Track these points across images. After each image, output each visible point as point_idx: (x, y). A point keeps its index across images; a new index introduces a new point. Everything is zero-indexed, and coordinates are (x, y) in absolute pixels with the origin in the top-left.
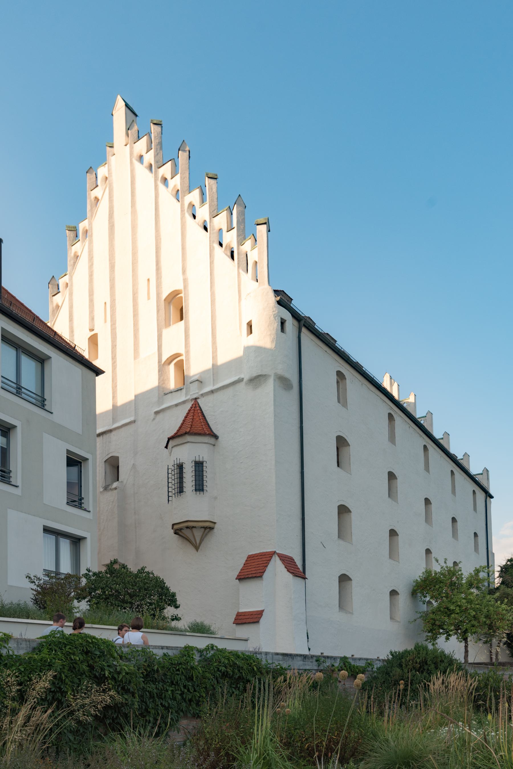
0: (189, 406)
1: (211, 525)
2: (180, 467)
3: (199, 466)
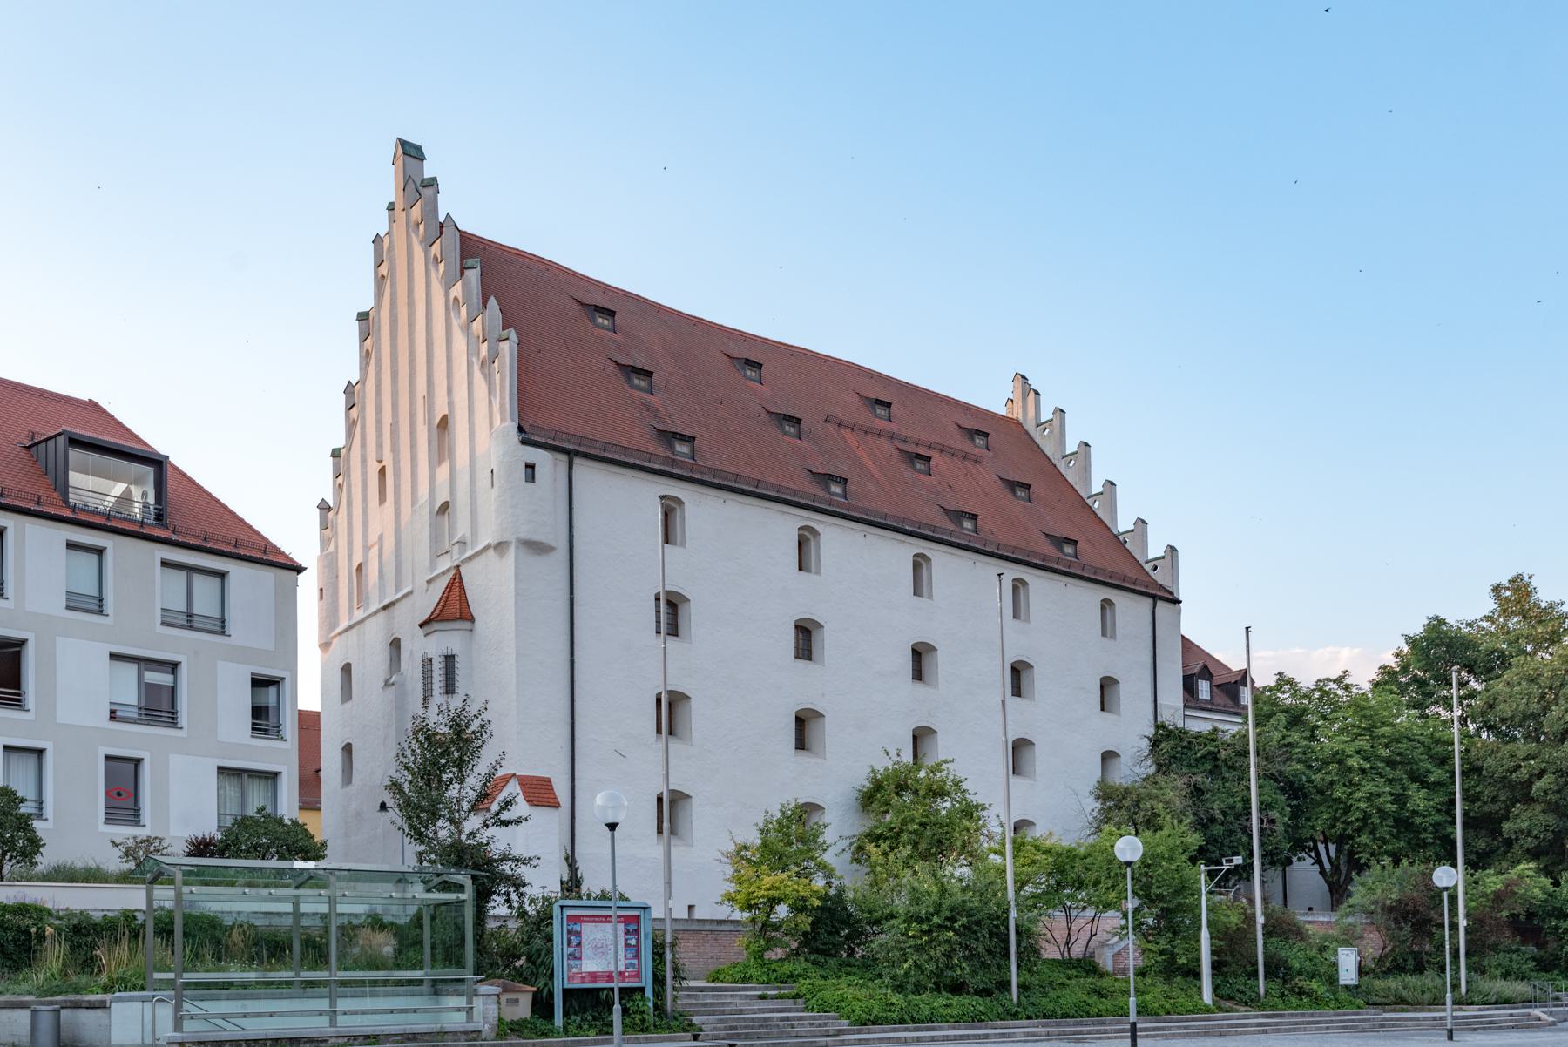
3: (449, 660)
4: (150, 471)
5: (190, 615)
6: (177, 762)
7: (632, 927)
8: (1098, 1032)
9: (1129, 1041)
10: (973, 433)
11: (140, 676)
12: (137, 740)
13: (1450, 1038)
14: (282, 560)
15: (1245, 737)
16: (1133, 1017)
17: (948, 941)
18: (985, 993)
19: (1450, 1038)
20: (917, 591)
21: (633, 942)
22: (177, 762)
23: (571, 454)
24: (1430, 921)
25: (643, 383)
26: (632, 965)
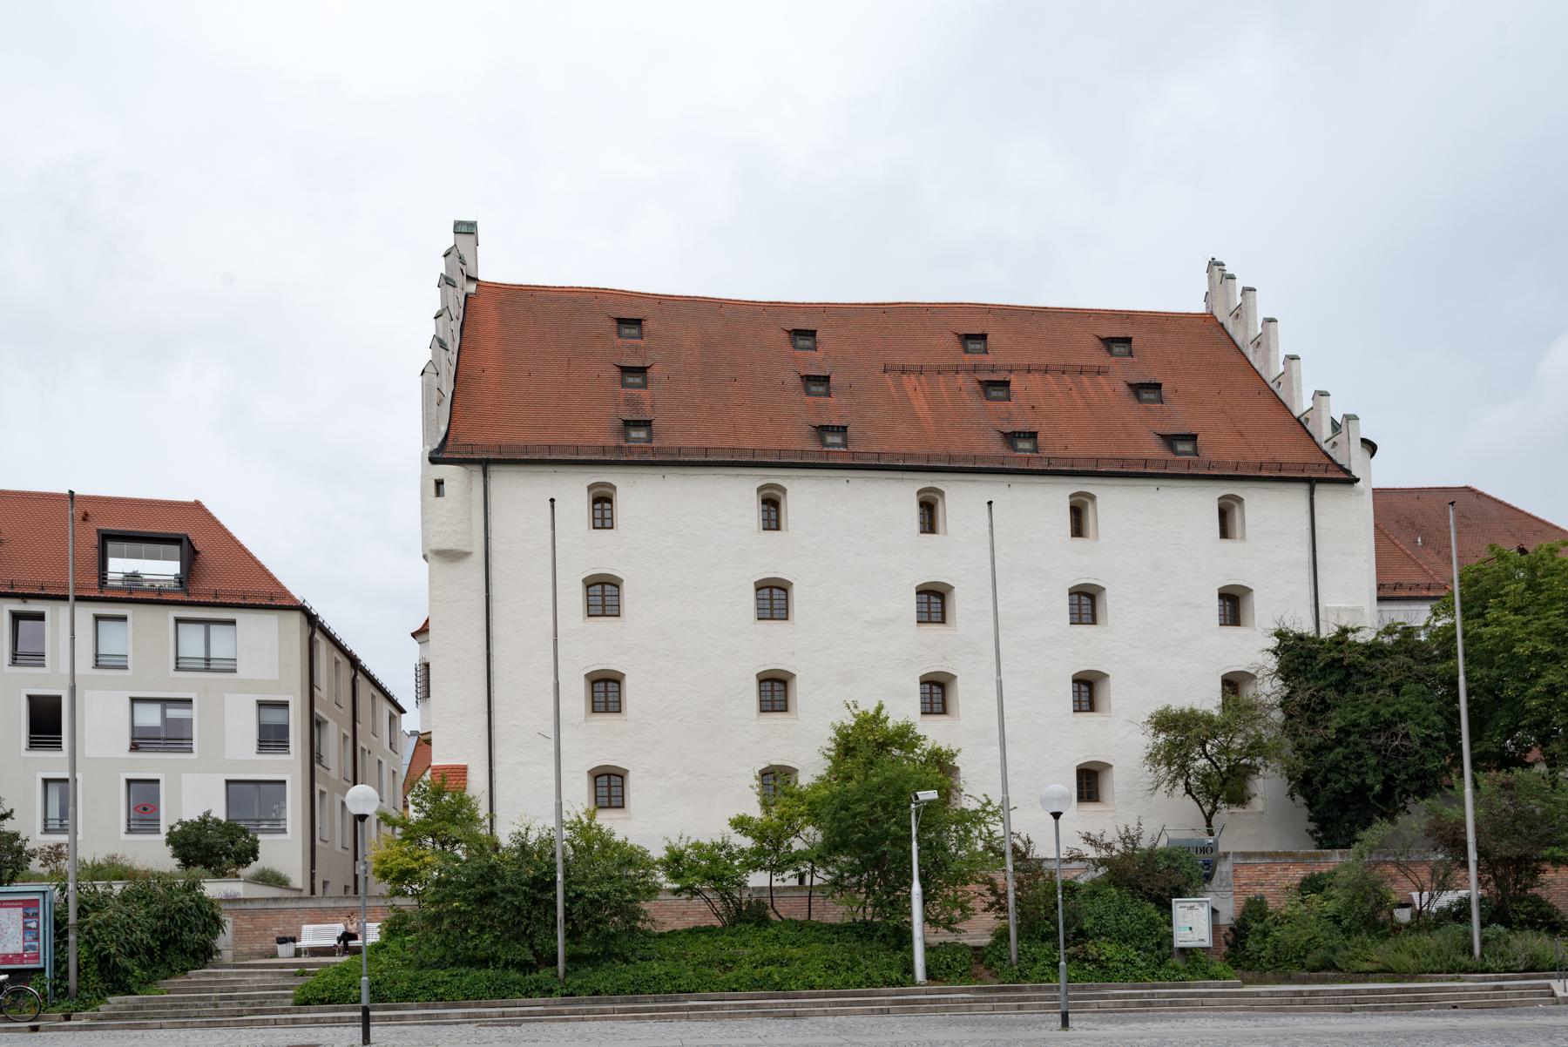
4: (176, 549)
5: (208, 659)
6: (188, 779)
7: (31, 911)
8: (666, 1009)
9: (357, 1032)
10: (1109, 342)
11: (164, 713)
12: (149, 765)
13: (1065, 1023)
14: (286, 603)
15: (1454, 626)
16: (365, 1002)
17: (457, 911)
18: (525, 967)
19: (1065, 1023)
20: (1224, 533)
21: (33, 925)
22: (188, 779)
23: (1312, 483)
24: (886, 835)
25: (1152, 396)
26: (33, 947)
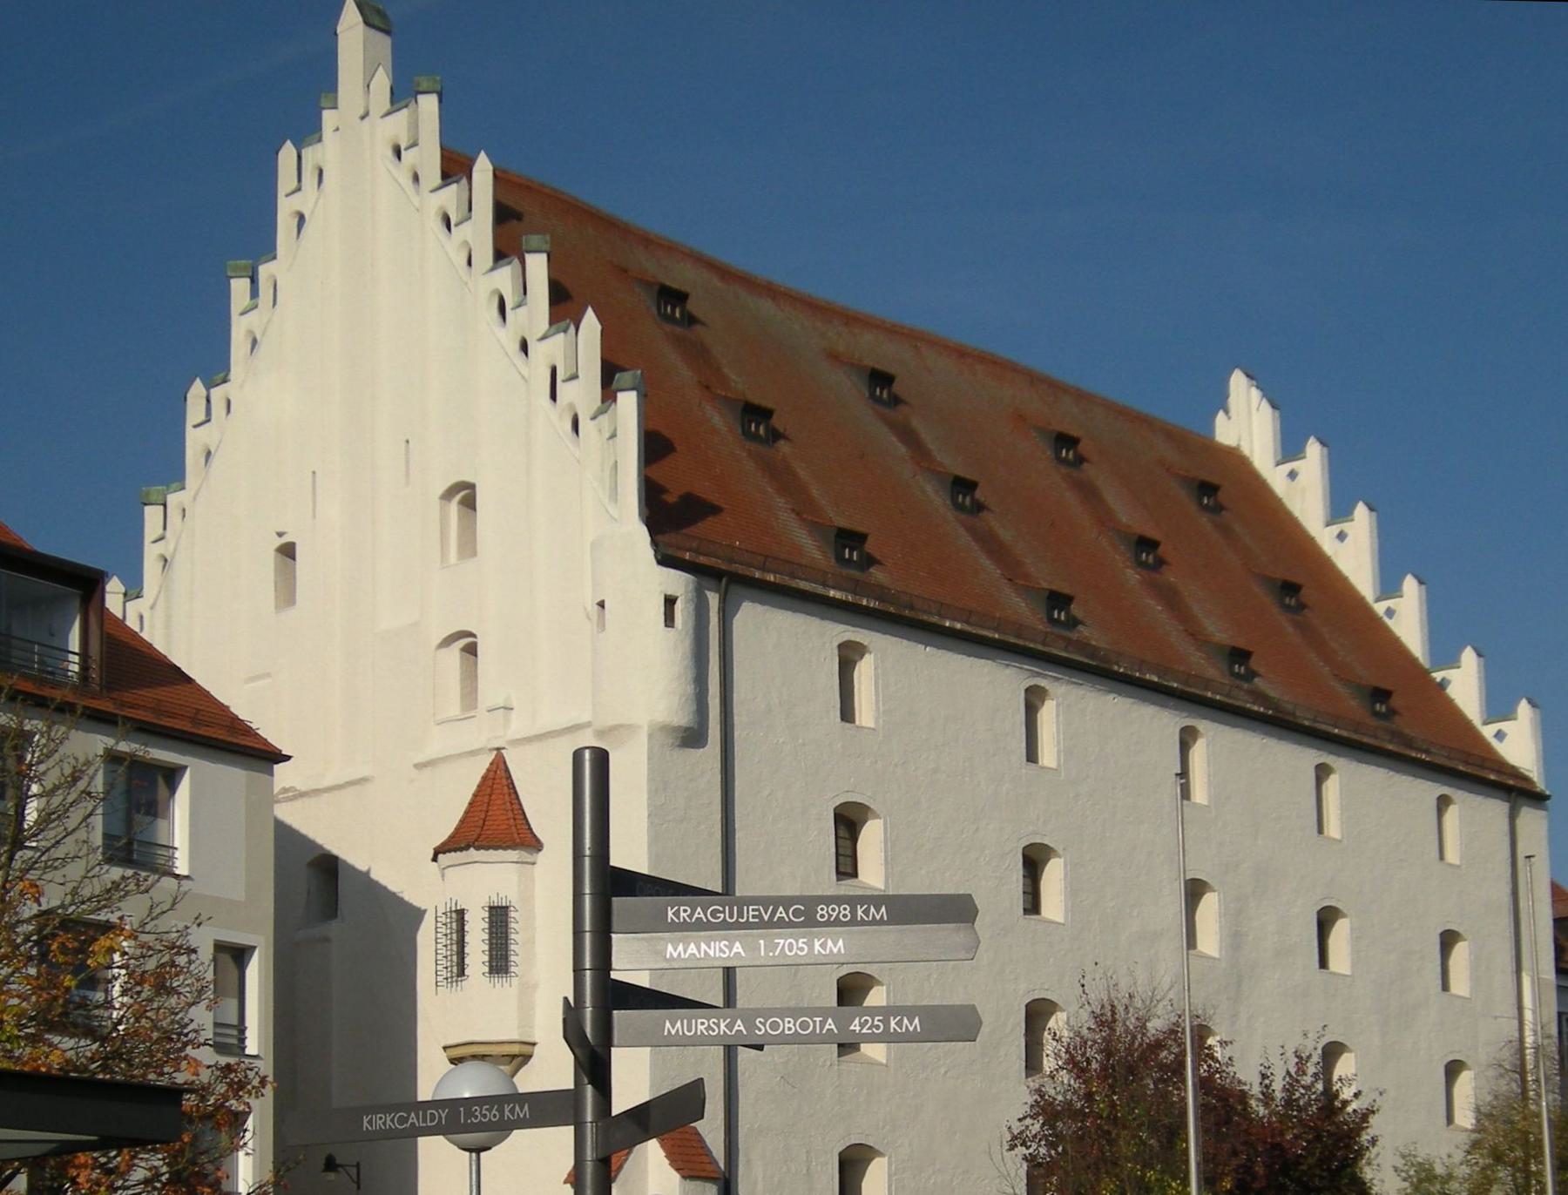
0: (482, 765)
1: (526, 1049)
2: (461, 914)
3: (499, 917)
